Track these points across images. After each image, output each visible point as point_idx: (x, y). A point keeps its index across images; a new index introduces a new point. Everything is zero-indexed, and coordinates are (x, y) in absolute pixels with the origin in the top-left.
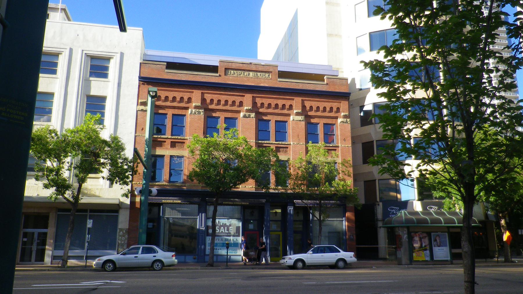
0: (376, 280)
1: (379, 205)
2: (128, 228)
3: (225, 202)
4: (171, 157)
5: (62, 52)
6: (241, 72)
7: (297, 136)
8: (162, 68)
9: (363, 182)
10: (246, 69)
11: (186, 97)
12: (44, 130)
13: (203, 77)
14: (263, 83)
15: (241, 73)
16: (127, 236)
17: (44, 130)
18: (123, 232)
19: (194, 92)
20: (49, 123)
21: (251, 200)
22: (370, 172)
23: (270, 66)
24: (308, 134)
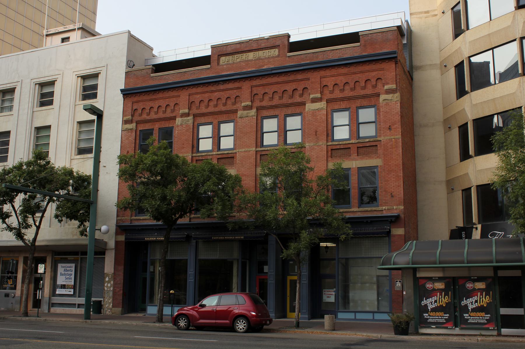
0: (191, 342)
1: (477, 228)
2: (113, 272)
3: (214, 237)
4: (359, 169)
5: (56, 77)
6: (238, 55)
7: (315, 133)
8: (147, 73)
9: (461, 191)
10: (245, 49)
11: (147, 106)
12: (25, 167)
13: (192, 74)
14: (266, 65)
15: (237, 57)
16: (112, 282)
17: (25, 167)
18: (109, 278)
19: (310, 79)
20: (5, 164)
21: (178, 235)
22: (465, 174)
23: (276, 37)
24: (375, 122)
